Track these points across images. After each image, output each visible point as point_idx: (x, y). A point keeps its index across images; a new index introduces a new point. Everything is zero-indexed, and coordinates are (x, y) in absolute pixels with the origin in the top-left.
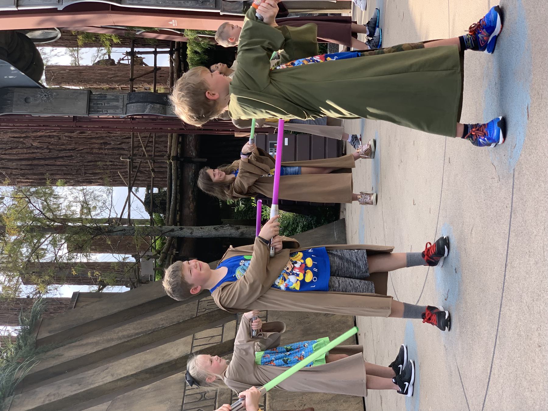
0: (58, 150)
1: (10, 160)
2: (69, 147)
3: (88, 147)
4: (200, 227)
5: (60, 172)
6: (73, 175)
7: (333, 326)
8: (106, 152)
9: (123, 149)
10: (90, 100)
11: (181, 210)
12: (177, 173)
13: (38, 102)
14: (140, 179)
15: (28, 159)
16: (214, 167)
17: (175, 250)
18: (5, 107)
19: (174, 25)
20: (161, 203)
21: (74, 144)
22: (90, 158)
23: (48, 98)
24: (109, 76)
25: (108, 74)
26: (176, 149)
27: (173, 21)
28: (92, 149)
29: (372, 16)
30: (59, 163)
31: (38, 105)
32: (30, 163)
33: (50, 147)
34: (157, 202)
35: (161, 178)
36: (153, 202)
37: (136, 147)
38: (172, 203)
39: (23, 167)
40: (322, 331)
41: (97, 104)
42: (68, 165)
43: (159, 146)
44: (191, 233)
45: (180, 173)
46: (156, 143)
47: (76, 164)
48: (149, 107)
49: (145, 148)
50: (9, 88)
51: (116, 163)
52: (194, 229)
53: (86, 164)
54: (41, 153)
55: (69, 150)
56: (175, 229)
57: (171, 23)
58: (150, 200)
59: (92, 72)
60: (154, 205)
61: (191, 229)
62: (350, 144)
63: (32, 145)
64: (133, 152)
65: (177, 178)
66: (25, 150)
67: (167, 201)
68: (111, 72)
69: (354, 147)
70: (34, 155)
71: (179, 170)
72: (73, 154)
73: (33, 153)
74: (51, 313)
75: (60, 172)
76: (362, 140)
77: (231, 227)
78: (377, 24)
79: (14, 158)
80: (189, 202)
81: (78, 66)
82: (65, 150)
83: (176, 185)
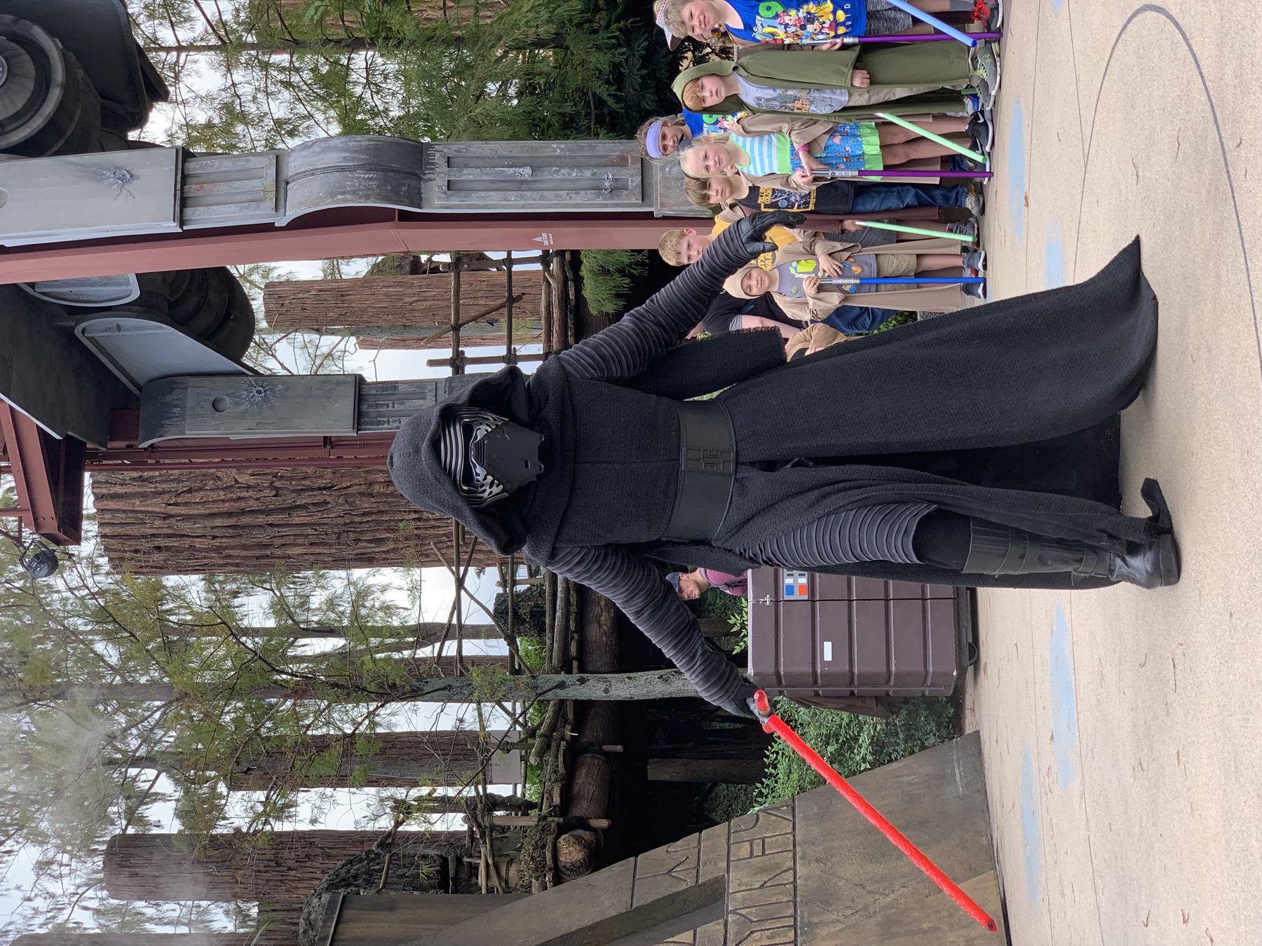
0: (296, 491)
1: (186, 518)
2: (321, 482)
4: (625, 675)
5: (300, 541)
6: (330, 545)
7: (951, 915)
13: (242, 408)
14: (483, 548)
15: (230, 514)
18: (168, 422)
20: (532, 615)
22: (366, 505)
23: (266, 399)
28: (371, 484)
30: (297, 520)
31: (242, 416)
32: (233, 521)
33: (278, 484)
34: (524, 611)
36: (515, 613)
38: (558, 614)
39: (216, 532)
40: (925, 926)
44: (606, 691)
50: (178, 379)
51: (425, 515)
52: (613, 682)
53: (357, 519)
56: (568, 683)
63: (237, 481)
66: (222, 493)
67: (548, 608)
68: (410, 291)
70: (243, 504)
72: (328, 499)
73: (239, 499)
74: (289, 869)
79: (196, 512)
80: (598, 609)
81: (337, 281)
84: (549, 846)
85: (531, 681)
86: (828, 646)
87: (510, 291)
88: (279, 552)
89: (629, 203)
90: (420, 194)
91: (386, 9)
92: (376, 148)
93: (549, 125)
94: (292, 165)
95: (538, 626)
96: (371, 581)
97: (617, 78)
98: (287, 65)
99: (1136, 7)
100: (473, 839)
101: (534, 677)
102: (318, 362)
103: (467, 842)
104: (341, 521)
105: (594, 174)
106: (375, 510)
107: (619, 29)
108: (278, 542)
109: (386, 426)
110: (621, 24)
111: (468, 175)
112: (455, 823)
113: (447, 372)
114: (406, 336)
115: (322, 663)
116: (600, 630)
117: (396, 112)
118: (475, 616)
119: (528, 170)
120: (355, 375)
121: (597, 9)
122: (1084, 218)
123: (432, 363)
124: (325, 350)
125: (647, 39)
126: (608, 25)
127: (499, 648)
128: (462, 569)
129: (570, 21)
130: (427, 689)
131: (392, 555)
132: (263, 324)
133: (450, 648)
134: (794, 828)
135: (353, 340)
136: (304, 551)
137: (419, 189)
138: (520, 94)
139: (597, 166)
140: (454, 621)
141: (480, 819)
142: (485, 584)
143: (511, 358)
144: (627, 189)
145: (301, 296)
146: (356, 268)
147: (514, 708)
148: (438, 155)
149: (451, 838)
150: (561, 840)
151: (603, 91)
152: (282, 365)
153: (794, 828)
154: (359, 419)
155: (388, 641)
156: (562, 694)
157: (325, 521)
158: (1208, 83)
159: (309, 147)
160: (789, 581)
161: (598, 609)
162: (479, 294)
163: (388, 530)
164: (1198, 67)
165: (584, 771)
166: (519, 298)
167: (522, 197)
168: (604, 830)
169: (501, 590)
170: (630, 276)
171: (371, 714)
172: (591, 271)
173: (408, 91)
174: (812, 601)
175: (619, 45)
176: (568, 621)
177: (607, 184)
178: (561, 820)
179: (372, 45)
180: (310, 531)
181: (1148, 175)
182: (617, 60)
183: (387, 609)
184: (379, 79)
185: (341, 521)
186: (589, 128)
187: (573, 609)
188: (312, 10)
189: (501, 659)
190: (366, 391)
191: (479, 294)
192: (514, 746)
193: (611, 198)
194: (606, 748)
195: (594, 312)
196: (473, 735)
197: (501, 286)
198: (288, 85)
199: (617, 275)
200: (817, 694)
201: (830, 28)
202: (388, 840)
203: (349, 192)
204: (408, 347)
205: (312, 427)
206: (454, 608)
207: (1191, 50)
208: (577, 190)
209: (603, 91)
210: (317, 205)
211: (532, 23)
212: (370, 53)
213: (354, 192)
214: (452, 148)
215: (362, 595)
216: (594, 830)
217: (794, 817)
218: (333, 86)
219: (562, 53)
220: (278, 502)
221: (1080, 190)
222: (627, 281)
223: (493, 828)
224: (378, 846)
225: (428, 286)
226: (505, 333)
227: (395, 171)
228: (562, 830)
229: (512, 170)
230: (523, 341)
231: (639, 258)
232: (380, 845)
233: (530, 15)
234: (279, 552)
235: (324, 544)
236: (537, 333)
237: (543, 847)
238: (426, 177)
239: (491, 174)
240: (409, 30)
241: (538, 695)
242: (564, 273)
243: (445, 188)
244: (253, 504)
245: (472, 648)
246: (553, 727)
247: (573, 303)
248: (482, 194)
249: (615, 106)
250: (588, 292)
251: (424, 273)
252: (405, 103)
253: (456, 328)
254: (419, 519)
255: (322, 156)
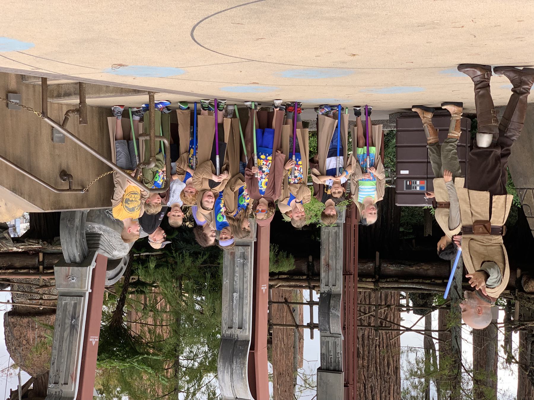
2: (362, 388)
6: (390, 386)
9: (363, 335)
10: (328, 370)
20: (423, 298)
22: (373, 369)
24: (283, 346)
26: (367, 283)
27: (262, 288)
28: (363, 366)
34: (421, 302)
35: (391, 298)
36: (422, 306)
37: (361, 323)
38: (423, 287)
43: (360, 299)
45: (391, 279)
47: (379, 383)
49: (366, 314)
51: (378, 343)
53: (379, 373)
57: (264, 291)
59: (279, 363)
60: (425, 305)
65: (397, 282)
67: (420, 292)
68: (279, 345)
71: (388, 280)
72: (369, 386)
83: (405, 283)
84: (529, 296)
86: (402, 172)
87: (282, 303)
89: (250, 251)
90: (243, 341)
91: (164, 351)
92: (223, 359)
93: (214, 283)
94: (229, 396)
95: (428, 296)
96: (405, 369)
98: (185, 394)
99: (191, 39)
100: (524, 329)
102: (308, 386)
103: (524, 332)
104: (379, 380)
105: (237, 266)
106: (375, 365)
107: (176, 252)
109: (340, 359)
111: (236, 320)
112: (516, 337)
113: (316, 332)
114: (298, 348)
115: (441, 391)
117: (206, 349)
118: (422, 325)
119: (235, 294)
120: (318, 371)
121: (167, 262)
122: (275, 61)
123: (312, 337)
124: (303, 382)
125: (180, 242)
126: (173, 257)
127: (435, 315)
128: (401, 328)
129: (171, 273)
130: (457, 347)
131: (395, 359)
133: (435, 335)
134: (530, 189)
135: (299, 370)
136: (392, 397)
137: (241, 341)
138: (200, 295)
139: (234, 265)
140: (423, 333)
141: (516, 326)
143: (311, 303)
144: (244, 253)
145: (280, 392)
146: (270, 369)
148: (227, 332)
149: (523, 338)
150: (526, 290)
153: (530, 189)
154: (337, 371)
155: (431, 362)
157: (379, 387)
158: (229, 8)
159: (222, 387)
160: (418, 188)
161: (421, 270)
162: (281, 315)
163: (384, 360)
164: (221, 12)
166: (285, 299)
167: (246, 297)
168: (522, 271)
170: (278, 252)
171: (467, 371)
172: (277, 268)
173: (197, 343)
174: (427, 178)
175: (182, 253)
176: (426, 283)
177: (242, 261)
178: (517, 290)
179: (178, 357)
180: (384, 394)
181: (262, 34)
182: (188, 254)
184: (192, 355)
185: (379, 380)
186: (215, 267)
187: (421, 281)
188: (163, 382)
189: (440, 312)
193: (248, 259)
195: (294, 267)
197: (278, 306)
198: (194, 394)
199: (278, 257)
201: (298, 167)
202: (523, 367)
204: (303, 346)
206: (420, 333)
207: (213, 15)
208: (244, 274)
210: (246, 386)
211: (172, 289)
212: (180, 357)
213: (242, 369)
214: (225, 327)
215: (413, 374)
216: (522, 276)
217: (525, 189)
218: (196, 375)
219: (183, 278)
221: (263, 63)
222: (281, 253)
223: (519, 320)
224: (527, 371)
225: (277, 337)
226: (298, 306)
228: (521, 290)
229: (235, 301)
231: (272, 247)
232: (526, 371)
233: (169, 290)
236: (299, 292)
237: (529, 298)
238: (236, 338)
239: (236, 310)
240: (173, 341)
241: (460, 298)
242: (275, 279)
243: (241, 330)
245: (435, 325)
247: (288, 276)
248: (244, 314)
249: (207, 256)
250: (286, 269)
251: (271, 338)
252: (202, 344)
253: (297, 326)
254: (379, 346)
255: (226, 382)
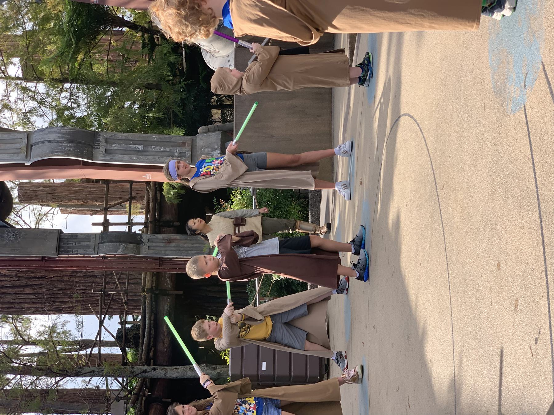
2: (39, 275)
3: (59, 275)
5: (28, 301)
8: (77, 279)
11: (155, 345)
12: (152, 307)
13: (5, 242)
16: (183, 403)
17: (147, 390)
19: (148, 178)
21: (44, 272)
22: (60, 286)
24: (84, 193)
25: (83, 191)
26: (150, 281)
27: (147, 175)
29: (357, 233)
30: (28, 292)
35: (135, 306)
36: (126, 337)
38: (145, 338)
41: (68, 244)
42: (37, 294)
43: (133, 273)
44: (165, 374)
45: (154, 306)
46: (129, 284)
48: (122, 247)
49: (118, 280)
52: (169, 370)
53: (55, 292)
54: (9, 281)
55: (39, 278)
56: (148, 370)
57: (144, 176)
58: (122, 335)
61: (165, 369)
62: (334, 362)
64: (105, 280)
65: (152, 312)
67: (141, 335)
68: (86, 190)
69: (339, 366)
71: (154, 303)
72: (42, 282)
75: (28, 301)
76: (348, 358)
77: (208, 366)
78: (363, 242)
82: (34, 278)
83: (150, 320)
85: (131, 369)
86: (264, 364)
88: (18, 306)
90: (92, 154)
95: (135, 345)
97: (183, 104)
101: (133, 368)
107: (184, 84)
108: (18, 301)
110: (186, 83)
111: (114, 147)
116: (163, 346)
118: (106, 337)
120: (58, 230)
123: (94, 224)
126: (180, 83)
127: (117, 351)
130: (83, 372)
132: (17, 200)
133: (95, 351)
135: (58, 209)
136: (30, 306)
139: (172, 146)
140: (98, 339)
142: (113, 324)
143: (130, 224)
144: (185, 157)
147: (123, 380)
148: (101, 138)
151: (177, 110)
152: (24, 221)
154: (59, 250)
156: (145, 375)
157: (40, 292)
161: (163, 337)
165: (153, 410)
169: (119, 326)
171: (56, 383)
177: (176, 154)
180: (33, 297)
183: (66, 333)
189: (119, 355)
190: (63, 237)
191: (118, 192)
192: (121, 398)
194: (163, 400)
196: (105, 391)
200: (258, 384)
203: (59, 152)
204: (83, 214)
205: (35, 253)
206: (98, 335)
209: (177, 110)
213: (62, 152)
220: (19, 283)
225: (94, 188)
226: (128, 210)
227: (81, 143)
229: (134, 146)
230: (136, 214)
234: (18, 306)
235: (40, 303)
238: (96, 147)
242: (156, 188)
244: (7, 284)
245: (105, 351)
246: (140, 390)
247: (159, 201)
254: (84, 293)
255: (48, 135)
